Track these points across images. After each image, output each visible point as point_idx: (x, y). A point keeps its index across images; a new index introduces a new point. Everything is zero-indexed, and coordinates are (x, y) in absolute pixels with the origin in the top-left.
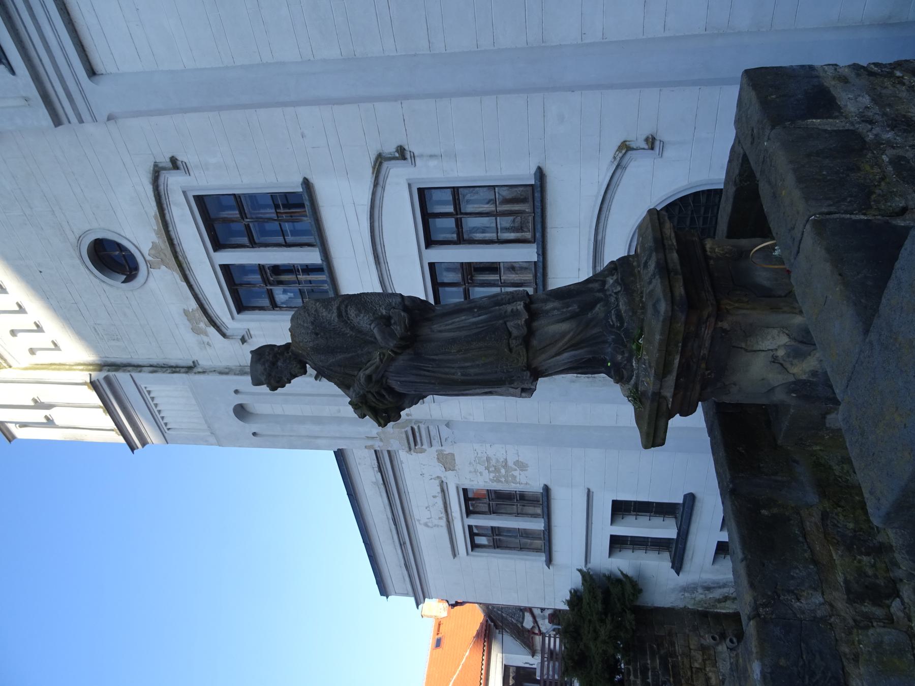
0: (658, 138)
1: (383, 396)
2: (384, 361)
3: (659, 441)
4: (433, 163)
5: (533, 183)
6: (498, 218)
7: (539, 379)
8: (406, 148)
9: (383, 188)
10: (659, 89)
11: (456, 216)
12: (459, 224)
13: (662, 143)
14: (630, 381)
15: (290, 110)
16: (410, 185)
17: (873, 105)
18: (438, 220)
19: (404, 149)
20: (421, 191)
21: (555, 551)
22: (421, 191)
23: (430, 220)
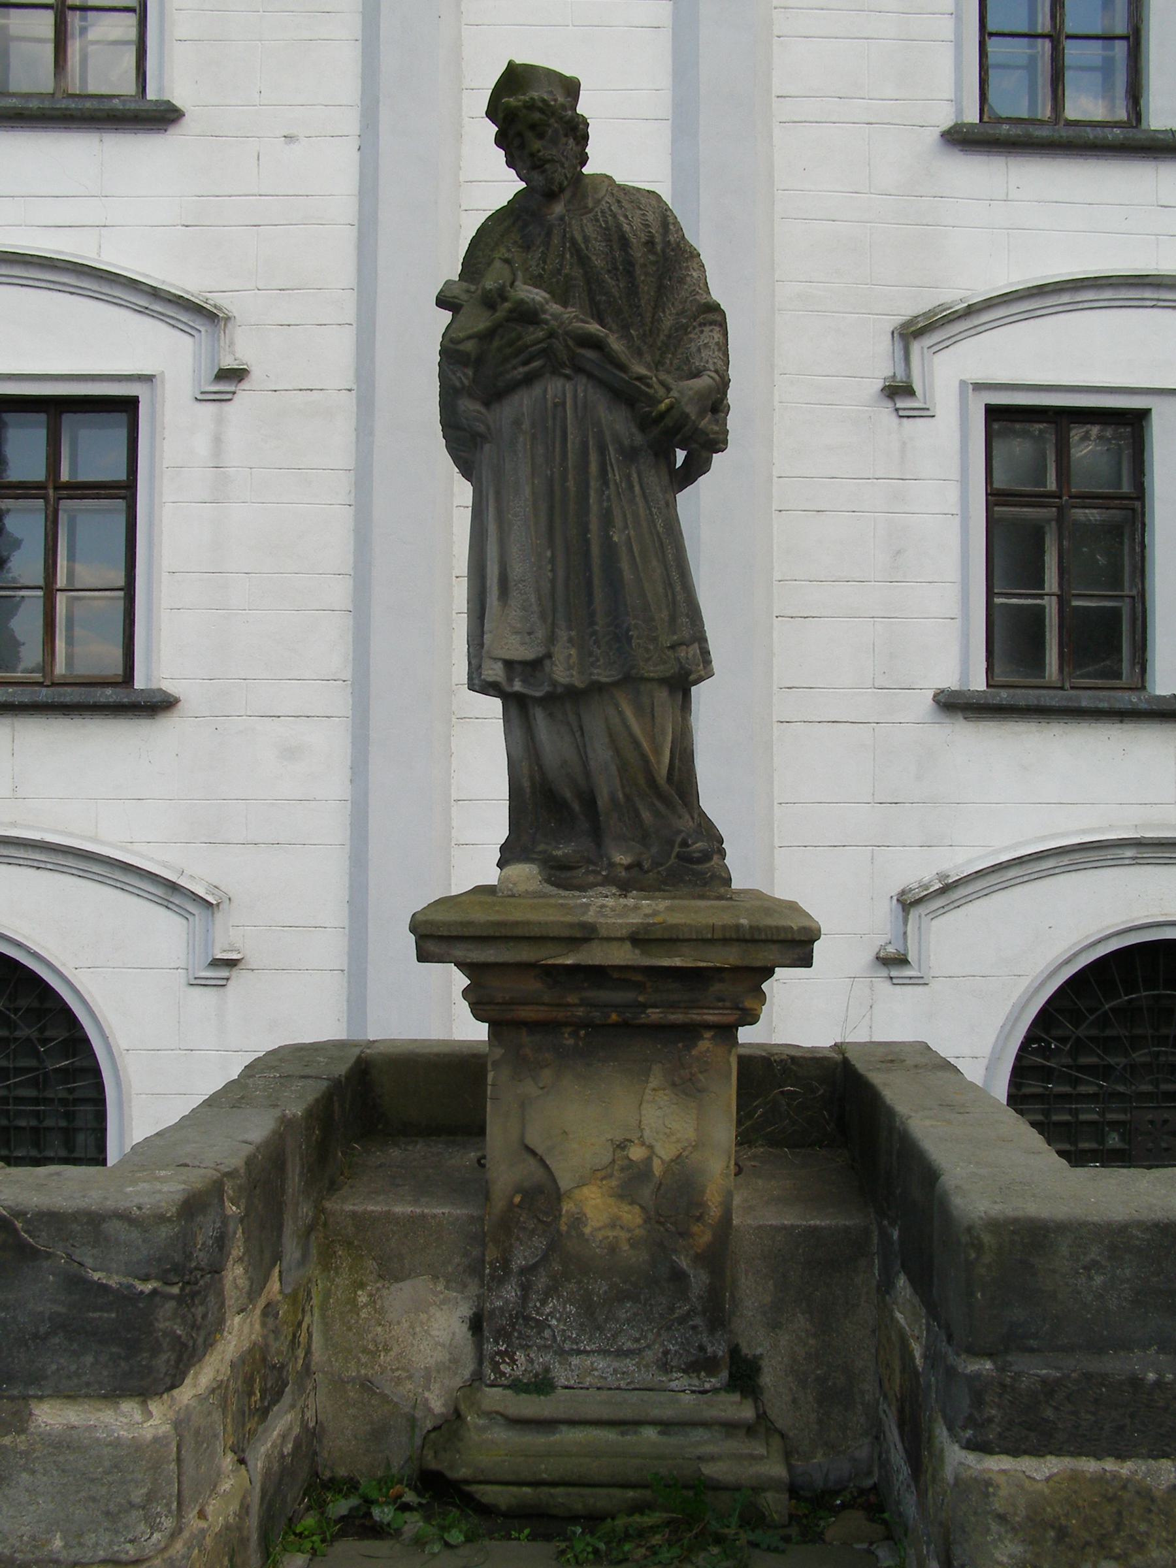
0: (235, 973)
1: (526, 363)
2: (638, 383)
3: (431, 947)
4: (202, 445)
5: (138, 684)
6: (40, 593)
7: (499, 699)
8: (245, 385)
9: (142, 311)
10: (346, 968)
11: (51, 485)
12: (24, 490)
13: (223, 982)
14: (553, 884)
15: (350, 122)
16: (148, 379)
17: (488, 1341)
18: (43, 433)
19: (241, 380)
20: (128, 406)
21: (13, 729)
22: (128, 406)
23: (43, 417)
